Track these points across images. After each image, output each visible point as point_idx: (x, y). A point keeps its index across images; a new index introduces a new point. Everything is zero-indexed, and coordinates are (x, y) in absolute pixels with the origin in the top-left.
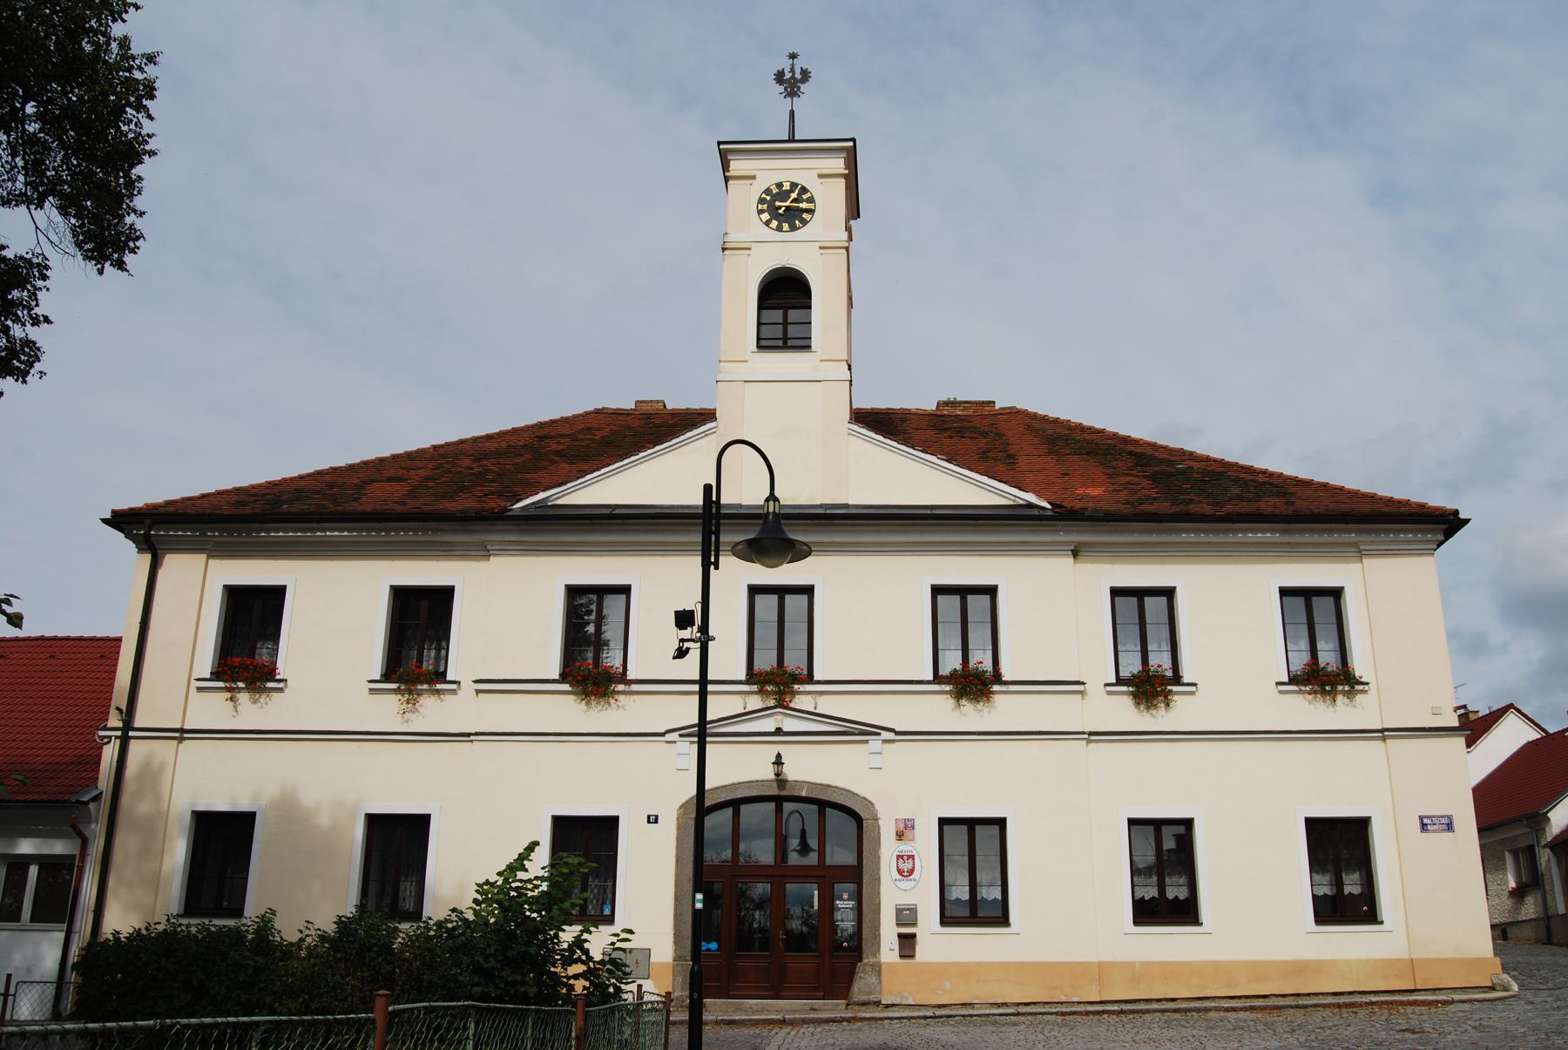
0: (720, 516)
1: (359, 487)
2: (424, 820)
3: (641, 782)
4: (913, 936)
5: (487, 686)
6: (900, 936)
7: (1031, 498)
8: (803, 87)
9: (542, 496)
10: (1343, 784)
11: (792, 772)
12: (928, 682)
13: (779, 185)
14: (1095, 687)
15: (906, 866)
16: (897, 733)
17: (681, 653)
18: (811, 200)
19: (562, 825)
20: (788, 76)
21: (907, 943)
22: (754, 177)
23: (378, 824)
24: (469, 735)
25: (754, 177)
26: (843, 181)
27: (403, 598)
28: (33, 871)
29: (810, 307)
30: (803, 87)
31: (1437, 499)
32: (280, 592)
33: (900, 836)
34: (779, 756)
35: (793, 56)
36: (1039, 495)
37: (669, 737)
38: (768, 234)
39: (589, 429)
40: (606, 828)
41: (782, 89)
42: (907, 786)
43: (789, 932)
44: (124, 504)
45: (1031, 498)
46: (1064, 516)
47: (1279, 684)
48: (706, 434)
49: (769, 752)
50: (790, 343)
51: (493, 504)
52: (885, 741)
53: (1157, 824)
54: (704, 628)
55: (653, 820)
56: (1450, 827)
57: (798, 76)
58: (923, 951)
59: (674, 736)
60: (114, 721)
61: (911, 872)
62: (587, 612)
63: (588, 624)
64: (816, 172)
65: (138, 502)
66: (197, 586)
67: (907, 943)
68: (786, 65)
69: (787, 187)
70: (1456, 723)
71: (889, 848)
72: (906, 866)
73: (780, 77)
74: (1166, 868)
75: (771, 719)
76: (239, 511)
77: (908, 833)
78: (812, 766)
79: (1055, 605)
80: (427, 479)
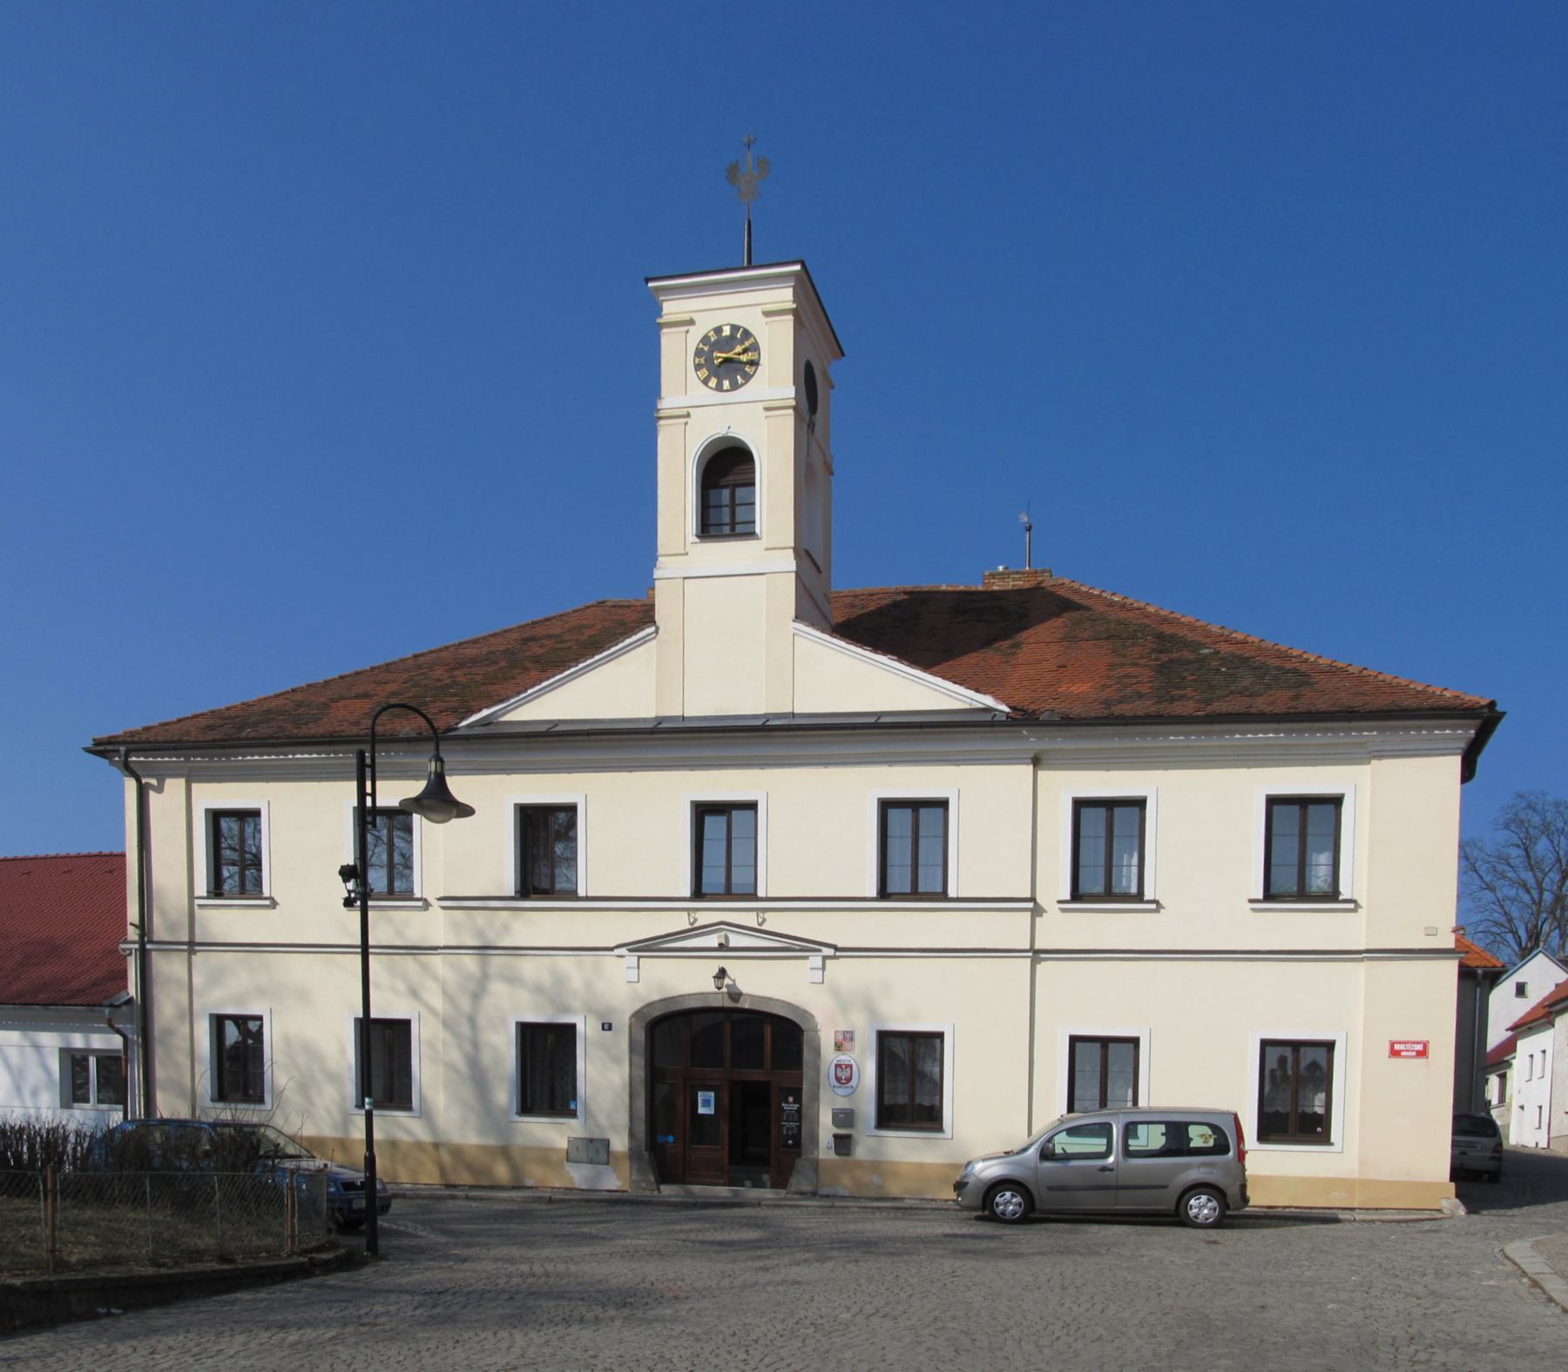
1: (325, 706)
2: (940, 1036)
4: (848, 1137)
5: (453, 902)
6: (836, 1137)
9: (485, 712)
10: (1299, 1007)
11: (745, 987)
13: (718, 330)
15: (844, 1075)
16: (836, 948)
18: (755, 347)
21: (843, 1143)
22: (691, 322)
23: (528, 1033)
24: (436, 948)
25: (691, 322)
26: (791, 317)
28: (92, 1061)
29: (753, 484)
36: (996, 697)
37: (617, 952)
42: (840, 1001)
44: (104, 734)
45: (988, 701)
46: (1023, 719)
47: (1251, 901)
48: (644, 641)
49: (713, 966)
50: (739, 529)
55: (607, 1027)
58: (861, 1152)
59: (623, 951)
60: (133, 933)
61: (849, 1079)
63: (544, 840)
64: (759, 310)
65: (118, 730)
66: (178, 813)
67: (843, 1143)
69: (727, 331)
70: (1451, 944)
75: (715, 936)
76: (210, 736)
77: (847, 1045)
78: (765, 983)
79: (1008, 816)
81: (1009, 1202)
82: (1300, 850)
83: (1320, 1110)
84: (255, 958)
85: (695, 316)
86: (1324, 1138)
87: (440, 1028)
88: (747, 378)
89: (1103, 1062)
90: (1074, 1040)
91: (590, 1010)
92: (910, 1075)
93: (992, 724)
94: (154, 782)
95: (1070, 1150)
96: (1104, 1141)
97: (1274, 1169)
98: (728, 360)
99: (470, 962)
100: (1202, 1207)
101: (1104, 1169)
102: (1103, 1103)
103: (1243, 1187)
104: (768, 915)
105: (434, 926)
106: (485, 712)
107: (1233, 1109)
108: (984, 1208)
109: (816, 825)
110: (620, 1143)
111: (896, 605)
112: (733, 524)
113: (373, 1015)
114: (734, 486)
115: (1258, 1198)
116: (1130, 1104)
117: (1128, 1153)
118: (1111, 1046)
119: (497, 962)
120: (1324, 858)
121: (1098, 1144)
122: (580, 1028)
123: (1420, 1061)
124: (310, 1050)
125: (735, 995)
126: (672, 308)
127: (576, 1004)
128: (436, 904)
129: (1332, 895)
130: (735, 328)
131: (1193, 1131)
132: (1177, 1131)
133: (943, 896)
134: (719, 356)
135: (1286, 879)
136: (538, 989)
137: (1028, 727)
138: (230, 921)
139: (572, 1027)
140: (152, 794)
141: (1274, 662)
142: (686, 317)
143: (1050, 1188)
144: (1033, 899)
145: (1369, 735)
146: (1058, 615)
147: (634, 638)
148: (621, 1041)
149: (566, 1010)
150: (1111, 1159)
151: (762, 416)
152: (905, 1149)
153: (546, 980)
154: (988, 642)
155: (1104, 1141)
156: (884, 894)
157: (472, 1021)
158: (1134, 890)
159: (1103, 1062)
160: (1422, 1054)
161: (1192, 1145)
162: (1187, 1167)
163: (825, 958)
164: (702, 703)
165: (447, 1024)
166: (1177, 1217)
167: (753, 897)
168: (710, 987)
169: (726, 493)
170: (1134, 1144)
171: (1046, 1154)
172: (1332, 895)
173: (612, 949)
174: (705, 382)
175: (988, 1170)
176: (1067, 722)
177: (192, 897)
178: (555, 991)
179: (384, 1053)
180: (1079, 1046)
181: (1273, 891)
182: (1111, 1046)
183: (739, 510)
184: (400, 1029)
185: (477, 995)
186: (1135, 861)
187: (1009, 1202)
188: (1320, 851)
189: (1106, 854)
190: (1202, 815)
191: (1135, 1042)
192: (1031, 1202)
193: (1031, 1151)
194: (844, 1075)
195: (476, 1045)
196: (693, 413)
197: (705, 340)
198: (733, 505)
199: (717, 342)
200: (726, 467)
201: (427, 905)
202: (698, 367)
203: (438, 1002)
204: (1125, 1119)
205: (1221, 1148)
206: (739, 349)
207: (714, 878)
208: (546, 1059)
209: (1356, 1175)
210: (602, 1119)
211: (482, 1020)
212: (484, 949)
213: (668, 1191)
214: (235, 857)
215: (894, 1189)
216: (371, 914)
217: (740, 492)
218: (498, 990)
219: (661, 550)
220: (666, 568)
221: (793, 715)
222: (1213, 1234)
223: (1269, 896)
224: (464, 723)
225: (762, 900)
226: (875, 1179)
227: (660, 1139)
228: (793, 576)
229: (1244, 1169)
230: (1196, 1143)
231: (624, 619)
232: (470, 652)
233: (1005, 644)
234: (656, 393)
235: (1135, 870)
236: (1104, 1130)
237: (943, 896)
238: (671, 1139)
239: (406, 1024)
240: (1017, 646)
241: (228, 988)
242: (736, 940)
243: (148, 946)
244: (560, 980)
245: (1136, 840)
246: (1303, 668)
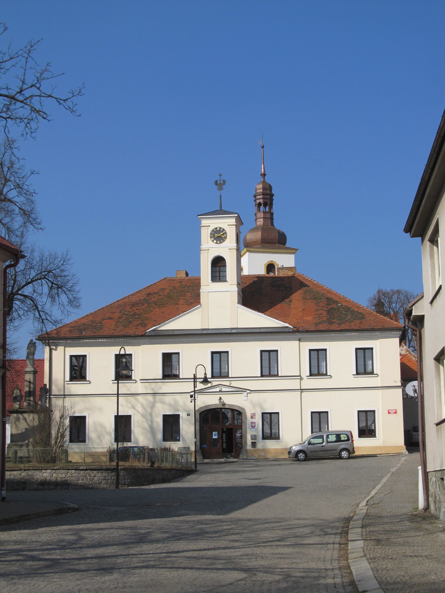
0: (196, 379)
4: (255, 442)
6: (252, 442)
7: (287, 325)
8: (224, 186)
9: (154, 328)
11: (226, 402)
12: (259, 377)
15: (253, 425)
16: (251, 391)
17: (191, 402)
18: (226, 233)
20: (219, 182)
22: (209, 226)
23: (166, 417)
25: (209, 226)
27: (118, 357)
29: (226, 266)
30: (224, 186)
32: (84, 357)
34: (220, 398)
35: (220, 175)
36: (289, 324)
41: (217, 187)
43: (150, 467)
45: (287, 325)
48: (198, 308)
49: (218, 397)
54: (195, 398)
55: (188, 415)
56: (395, 413)
57: (222, 182)
61: (255, 426)
62: (168, 360)
68: (218, 178)
77: (254, 417)
78: (232, 400)
79: (293, 354)
80: (120, 318)
81: (301, 456)
82: (364, 363)
83: (373, 428)
84: (85, 399)
85: (210, 225)
86: (374, 436)
87: (140, 416)
88: (224, 241)
89: (319, 418)
90: (312, 413)
91: (185, 410)
93: (289, 332)
94: (54, 347)
95: (315, 442)
96: (322, 440)
97: (361, 444)
98: (218, 236)
99: (150, 398)
100: (344, 454)
101: (323, 446)
102: (320, 431)
103: (353, 449)
104: (232, 382)
105: (139, 388)
106: (154, 328)
107: (350, 430)
108: (296, 458)
109: (244, 358)
110: (193, 448)
111: (254, 282)
112: (220, 276)
113: (119, 414)
114: (220, 267)
115: (357, 453)
116: (327, 430)
117: (328, 442)
118: (321, 414)
119: (158, 397)
120: (370, 362)
121: (320, 440)
122: (181, 415)
123: (395, 414)
124: (102, 426)
125: (224, 404)
126: (204, 222)
127: (181, 408)
128: (139, 381)
129: (372, 373)
130: (220, 228)
131: (342, 436)
132: (338, 436)
133: (277, 375)
134: (217, 235)
135: (361, 370)
136: (170, 405)
138: (77, 388)
139: (179, 415)
140: (53, 351)
141: (356, 310)
142: (208, 225)
143: (311, 452)
144: (300, 376)
146: (300, 289)
147: (195, 308)
148: (192, 418)
149: (178, 410)
150: (324, 444)
152: (271, 445)
153: (172, 402)
154: (283, 299)
155: (322, 440)
156: (262, 376)
157: (151, 415)
158: (325, 373)
159: (319, 418)
160: (395, 413)
161: (342, 439)
162: (342, 444)
163: (248, 393)
165: (143, 416)
166: (340, 458)
167: (227, 377)
168: (218, 402)
169: (218, 268)
170: (329, 440)
171: (310, 443)
172: (372, 373)
174: (213, 241)
175: (296, 449)
176: (307, 331)
177: (64, 381)
178: (175, 405)
179: (123, 424)
180: (313, 414)
181: (358, 372)
182: (321, 414)
183: (221, 273)
184: (128, 418)
185: (153, 407)
186: (325, 365)
187: (301, 456)
188: (369, 360)
189: (318, 364)
190: (341, 352)
191: (327, 412)
192: (305, 455)
193: (306, 443)
194: (253, 426)
195: (152, 422)
196: (210, 250)
197: (213, 231)
198: (220, 272)
199: (216, 231)
200: (218, 263)
201: (136, 382)
202: (211, 237)
203: (140, 409)
204: (327, 434)
205: (348, 440)
206: (222, 234)
207: (217, 370)
208: (171, 424)
209: (382, 445)
210: (188, 441)
211: (154, 414)
212: (154, 394)
213: (206, 461)
214: (78, 370)
215: (269, 456)
216: (120, 384)
217: (221, 268)
218: (159, 406)
219: (201, 285)
220: (203, 290)
221: (238, 328)
222: (347, 460)
223: (358, 373)
224: (148, 331)
225: (230, 378)
226: (263, 454)
227: (203, 446)
228: (237, 292)
229: (353, 444)
230: (342, 439)
232: (134, 299)
233: (287, 300)
234: (200, 244)
235: (325, 367)
236: (322, 437)
237: (277, 375)
238: (206, 446)
239: (130, 416)
240: (290, 301)
241: (78, 409)
242: (224, 389)
243: (51, 396)
244: (176, 402)
245: (325, 359)
246: (363, 312)
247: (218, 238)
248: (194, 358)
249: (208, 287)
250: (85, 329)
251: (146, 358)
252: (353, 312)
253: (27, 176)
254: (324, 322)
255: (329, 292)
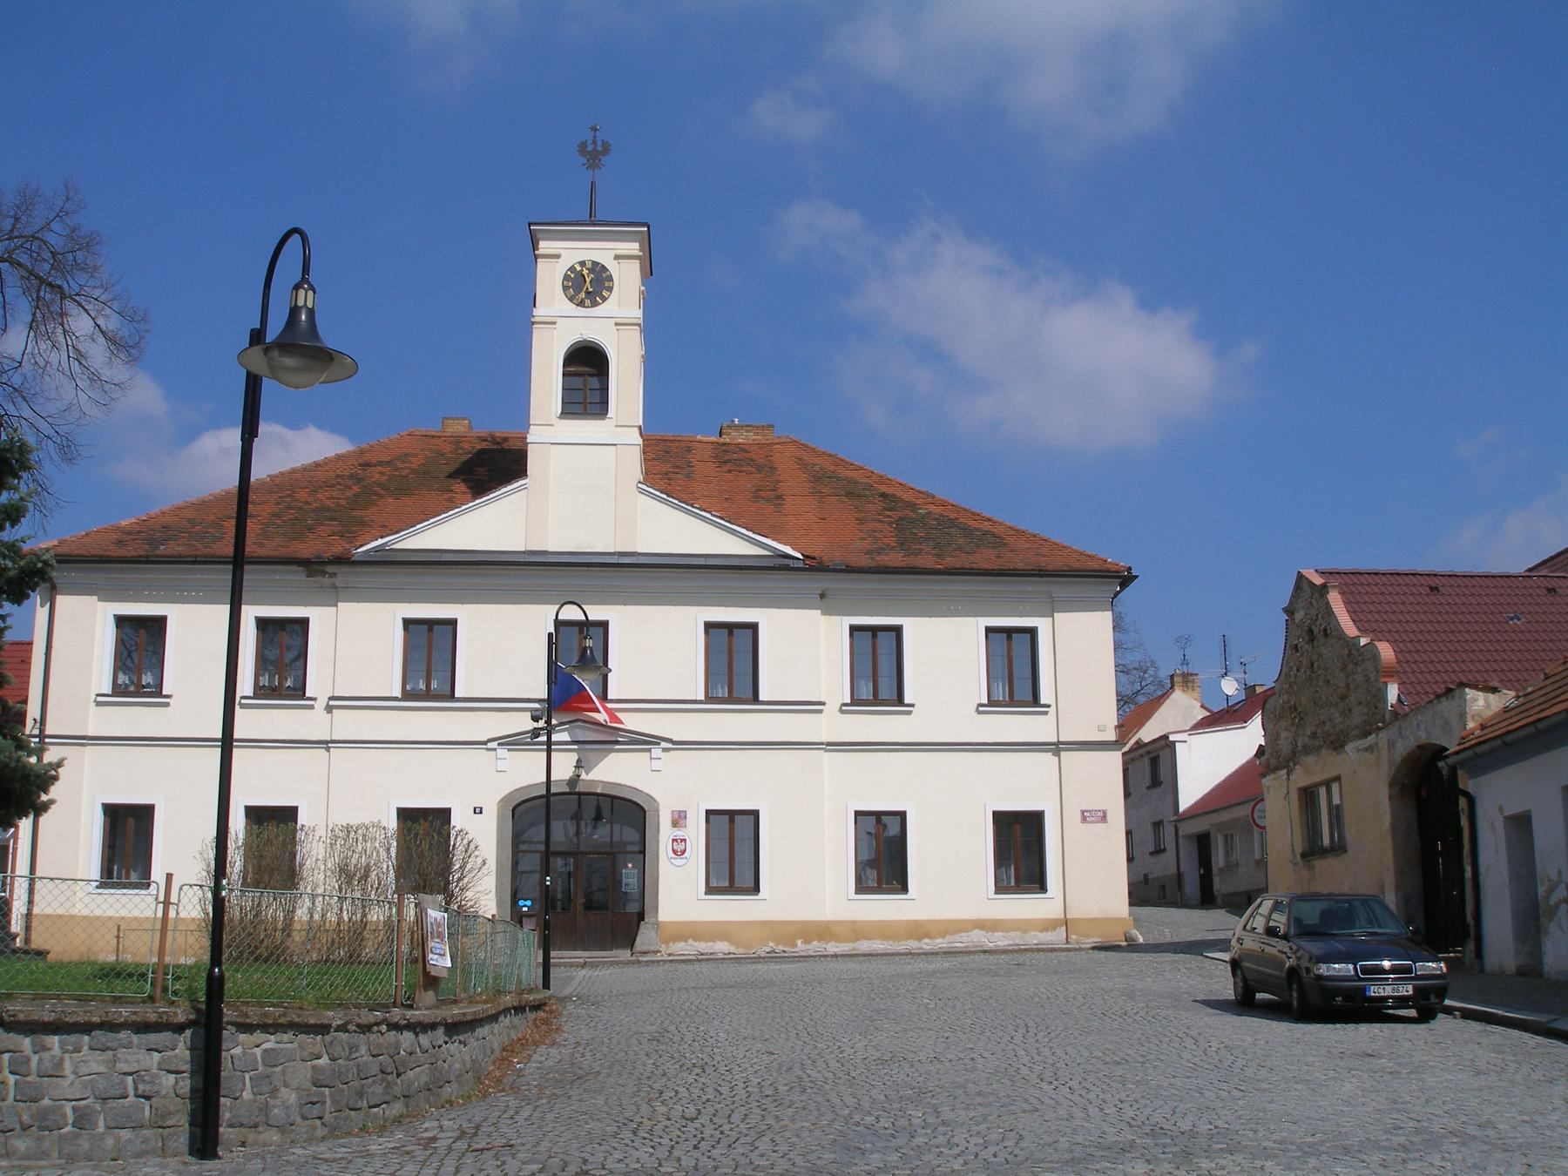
2: (904, 889)
3: (478, 782)
9: (380, 541)
10: (1024, 785)
12: (700, 702)
14: (832, 708)
15: (679, 847)
19: (405, 815)
20: (590, 148)
22: (558, 256)
23: (407, 816)
25: (558, 256)
31: (1116, 558)
33: (675, 824)
37: (490, 745)
38: (571, 308)
39: (406, 455)
40: (1034, 821)
42: (680, 786)
46: (814, 566)
51: (337, 548)
52: (665, 750)
53: (878, 815)
55: (478, 811)
56: (1104, 819)
57: (599, 148)
59: (494, 745)
61: (684, 852)
64: (613, 253)
71: (666, 833)
72: (679, 847)
73: (582, 148)
74: (883, 853)
78: (616, 771)
79: (804, 646)
80: (275, 515)
82: (1015, 675)
92: (735, 846)
106: (380, 541)
126: (545, 246)
137: (809, 576)
145: (1060, 589)
151: (617, 326)
164: (559, 539)
173: (485, 743)
176: (850, 570)
189: (878, 674)
196: (559, 325)
200: (587, 363)
231: (496, 465)
247: (588, 294)
248: (505, 647)
249: (550, 431)
250: (165, 541)
251: (356, 640)
252: (967, 532)
253: (658, 957)
254: (892, 548)
255: (882, 479)
